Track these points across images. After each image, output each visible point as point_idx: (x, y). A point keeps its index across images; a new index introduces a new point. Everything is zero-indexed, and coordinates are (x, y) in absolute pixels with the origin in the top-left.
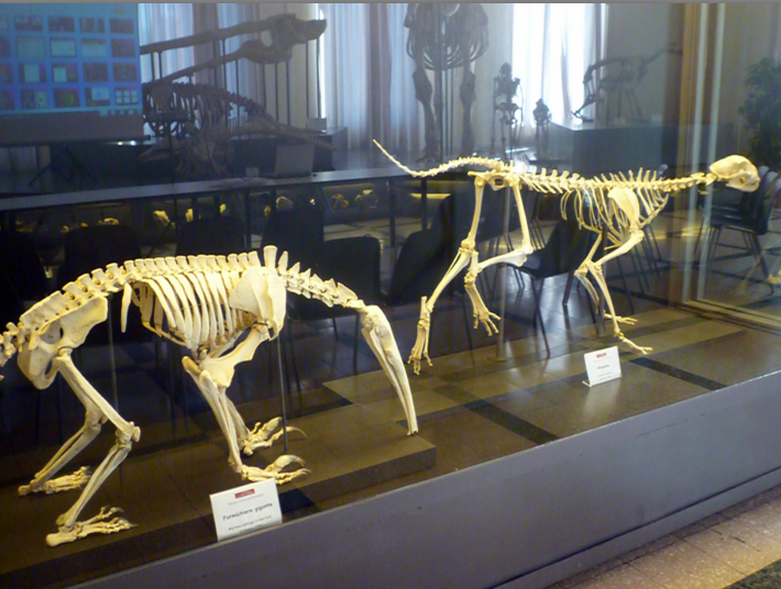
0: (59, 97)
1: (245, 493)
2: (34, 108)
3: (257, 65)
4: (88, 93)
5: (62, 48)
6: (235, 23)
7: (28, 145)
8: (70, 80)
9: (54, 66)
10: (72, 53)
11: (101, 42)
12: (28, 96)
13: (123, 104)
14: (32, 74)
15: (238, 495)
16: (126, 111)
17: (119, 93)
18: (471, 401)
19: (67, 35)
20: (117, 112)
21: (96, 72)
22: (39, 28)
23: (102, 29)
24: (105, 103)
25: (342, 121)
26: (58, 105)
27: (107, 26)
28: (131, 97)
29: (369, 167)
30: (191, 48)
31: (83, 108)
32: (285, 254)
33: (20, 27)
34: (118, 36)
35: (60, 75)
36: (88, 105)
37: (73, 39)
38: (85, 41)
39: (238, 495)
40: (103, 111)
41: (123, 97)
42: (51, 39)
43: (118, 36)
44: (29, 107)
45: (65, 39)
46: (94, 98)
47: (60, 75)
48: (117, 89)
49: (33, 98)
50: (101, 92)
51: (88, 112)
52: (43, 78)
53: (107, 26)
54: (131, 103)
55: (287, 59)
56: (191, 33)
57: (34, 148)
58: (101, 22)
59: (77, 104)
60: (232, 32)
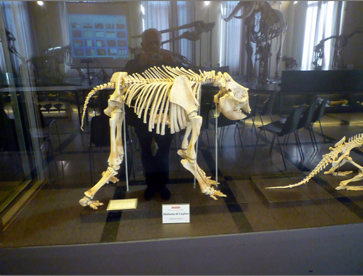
0: (99, 52)
1: (176, 208)
2: (90, 55)
3: (189, 41)
4: (109, 51)
5: (100, 35)
6: (185, 23)
7: (111, 68)
8: (103, 46)
9: (97, 41)
10: (103, 36)
11: (113, 32)
12: (88, 51)
13: (122, 55)
14: (90, 44)
15: (173, 208)
16: (123, 58)
17: (120, 51)
18: (340, 197)
19: (102, 30)
20: (120, 58)
21: (112, 43)
22: (91, 27)
23: (113, 28)
24: (115, 54)
25: (228, 63)
26: (98, 55)
27: (115, 26)
28: (124, 52)
29: (23, 92)
30: (168, 33)
31: (107, 56)
32: (150, 130)
33: (85, 27)
34: (119, 30)
35: (99, 44)
36: (109, 55)
37: (103, 31)
38: (107, 32)
39: (173, 208)
40: (114, 57)
41: (122, 52)
42: (96, 31)
43: (119, 30)
44: (89, 55)
45: (111, 32)
46: (111, 52)
47: (99, 44)
48: (120, 50)
49: (90, 52)
50: (113, 51)
51: (109, 58)
52: (93, 45)
53: (115, 26)
54: (122, 55)
55: (200, 38)
56: (168, 28)
57: (112, 69)
58: (113, 25)
59: (105, 54)
60: (183, 27)
